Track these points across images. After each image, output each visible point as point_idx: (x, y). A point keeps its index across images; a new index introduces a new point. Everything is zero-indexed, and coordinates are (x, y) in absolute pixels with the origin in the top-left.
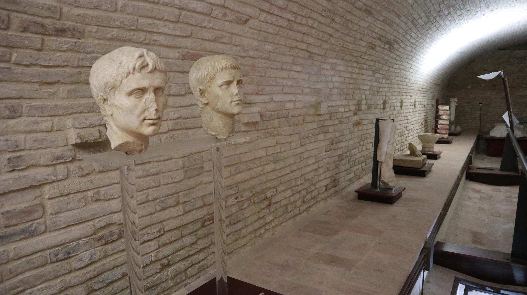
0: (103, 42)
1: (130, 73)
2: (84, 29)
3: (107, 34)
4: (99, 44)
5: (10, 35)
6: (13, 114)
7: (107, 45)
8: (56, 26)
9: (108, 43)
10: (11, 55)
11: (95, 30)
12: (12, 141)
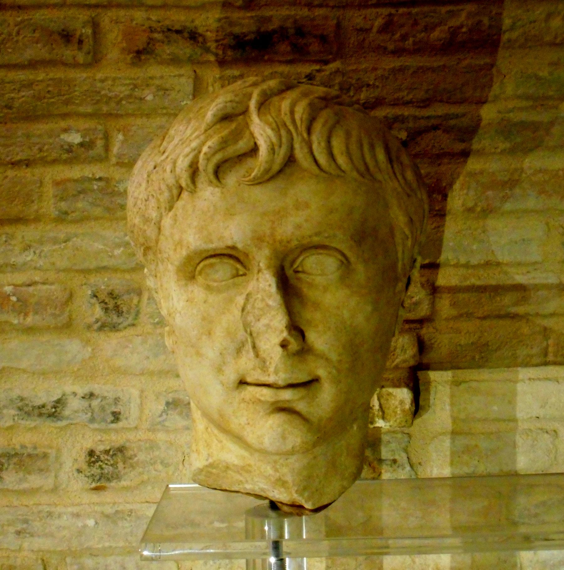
0: (412, 62)
1: (181, 189)
2: (338, 26)
3: (429, 28)
4: (402, 69)
5: (102, 81)
6: (115, 318)
7: (433, 70)
8: (237, 30)
9: (437, 62)
10: (107, 137)
11: (379, 22)
12: (105, 398)
